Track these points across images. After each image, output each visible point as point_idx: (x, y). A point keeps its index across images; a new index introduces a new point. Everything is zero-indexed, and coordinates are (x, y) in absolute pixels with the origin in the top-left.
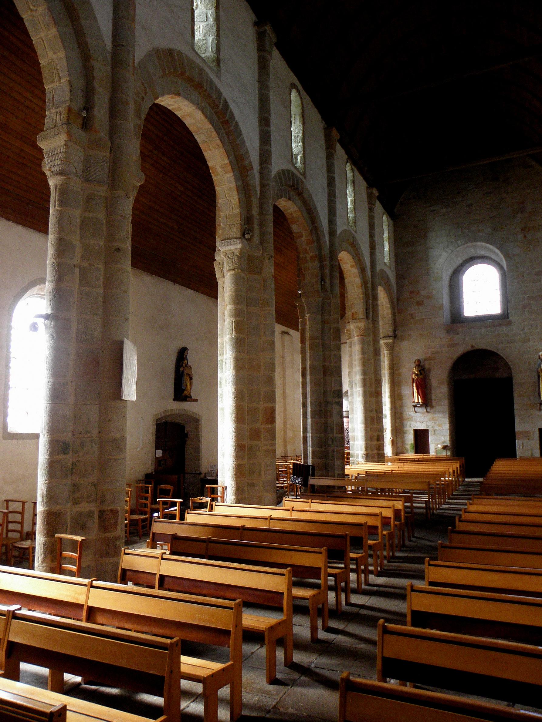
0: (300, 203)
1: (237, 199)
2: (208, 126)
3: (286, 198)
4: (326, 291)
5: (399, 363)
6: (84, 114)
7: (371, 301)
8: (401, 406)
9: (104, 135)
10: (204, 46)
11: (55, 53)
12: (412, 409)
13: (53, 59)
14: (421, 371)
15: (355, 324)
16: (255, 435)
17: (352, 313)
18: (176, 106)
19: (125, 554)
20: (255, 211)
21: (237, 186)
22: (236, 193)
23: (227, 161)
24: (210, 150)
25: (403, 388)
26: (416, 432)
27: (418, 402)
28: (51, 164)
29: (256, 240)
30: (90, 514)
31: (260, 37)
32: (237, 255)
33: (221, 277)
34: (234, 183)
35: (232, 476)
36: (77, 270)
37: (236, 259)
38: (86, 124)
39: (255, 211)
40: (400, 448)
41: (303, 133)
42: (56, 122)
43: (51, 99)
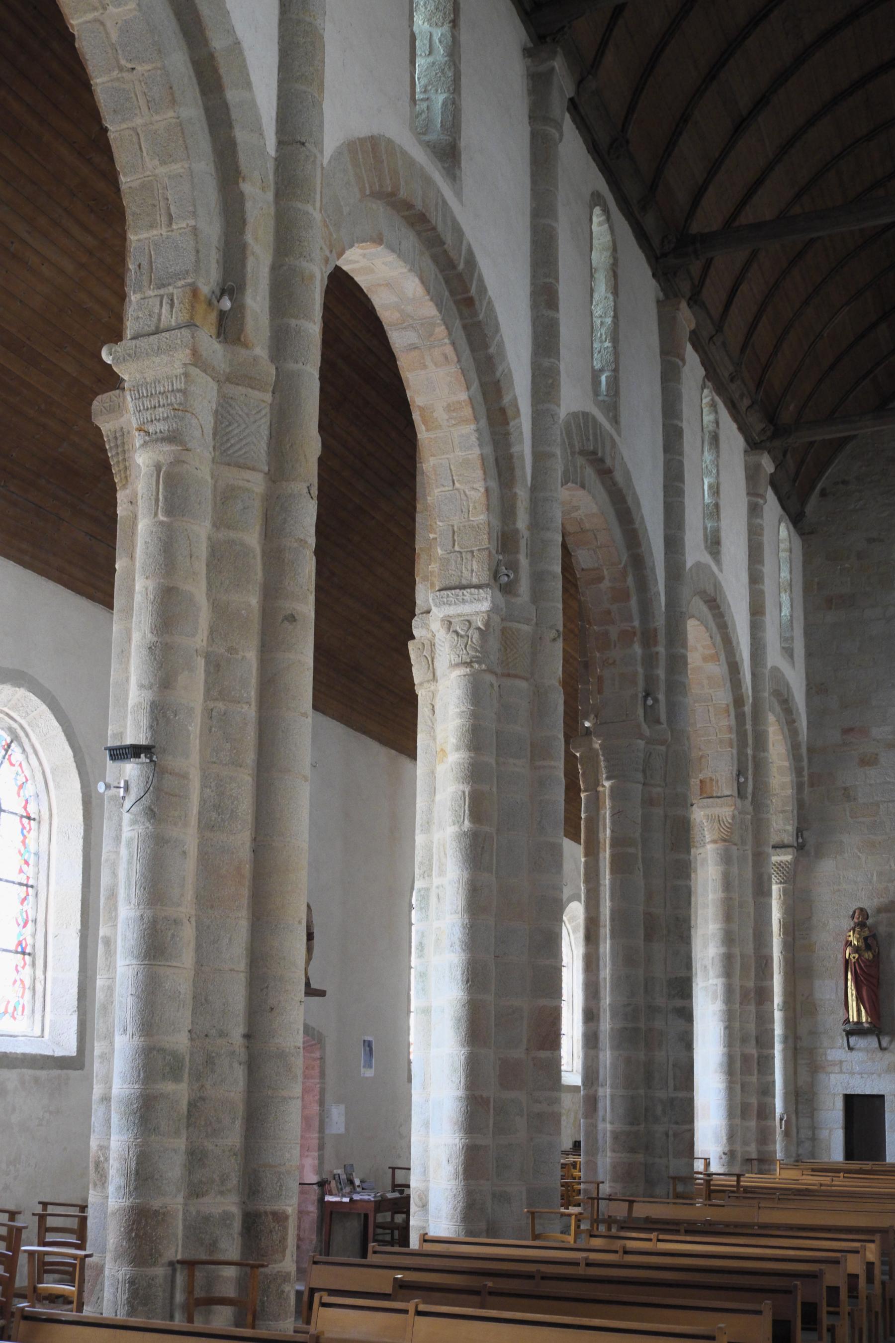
0: (602, 495)
1: (482, 490)
2: (430, 310)
3: (576, 484)
4: (658, 722)
5: (810, 918)
6: (226, 304)
7: (750, 752)
8: (814, 1033)
9: (261, 351)
10: (424, 116)
11: (163, 163)
12: (841, 1040)
13: (155, 176)
14: (869, 941)
15: (708, 811)
16: (509, 1074)
17: (701, 781)
18: (364, 263)
19: (324, 1305)
20: (522, 522)
21: (483, 458)
22: (479, 473)
23: (463, 396)
24: (425, 367)
25: (817, 983)
26: (850, 1101)
27: (859, 1022)
28: (148, 415)
29: (524, 587)
30: (226, 1217)
31: (539, 84)
32: (479, 629)
33: (428, 681)
34: (477, 451)
35: (457, 1173)
36: (201, 662)
37: (476, 636)
38: (229, 328)
39: (522, 522)
40: (807, 1144)
41: (615, 317)
42: (159, 320)
43: (145, 264)
